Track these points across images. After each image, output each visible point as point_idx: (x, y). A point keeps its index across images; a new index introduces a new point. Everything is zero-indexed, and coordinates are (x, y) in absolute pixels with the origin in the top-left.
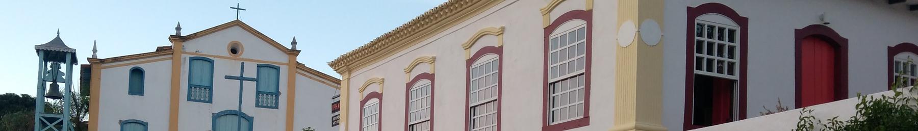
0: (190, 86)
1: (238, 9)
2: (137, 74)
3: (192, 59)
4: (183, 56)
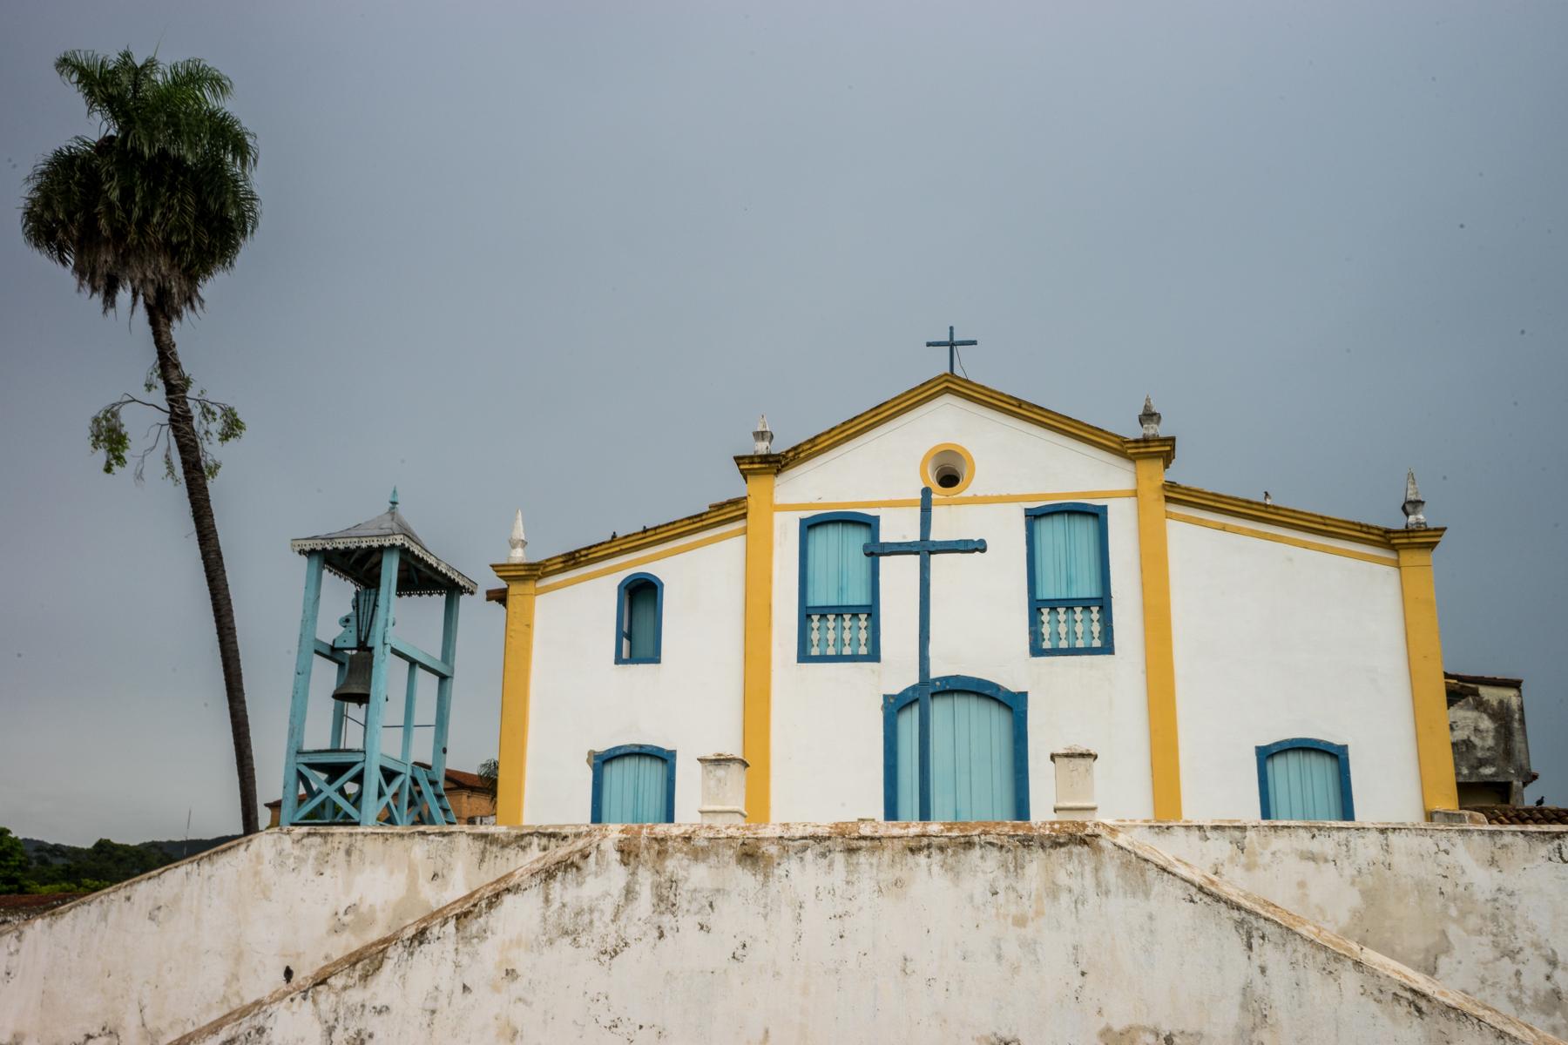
0: (806, 614)
1: (952, 345)
2: (641, 594)
3: (809, 526)
4: (779, 518)
